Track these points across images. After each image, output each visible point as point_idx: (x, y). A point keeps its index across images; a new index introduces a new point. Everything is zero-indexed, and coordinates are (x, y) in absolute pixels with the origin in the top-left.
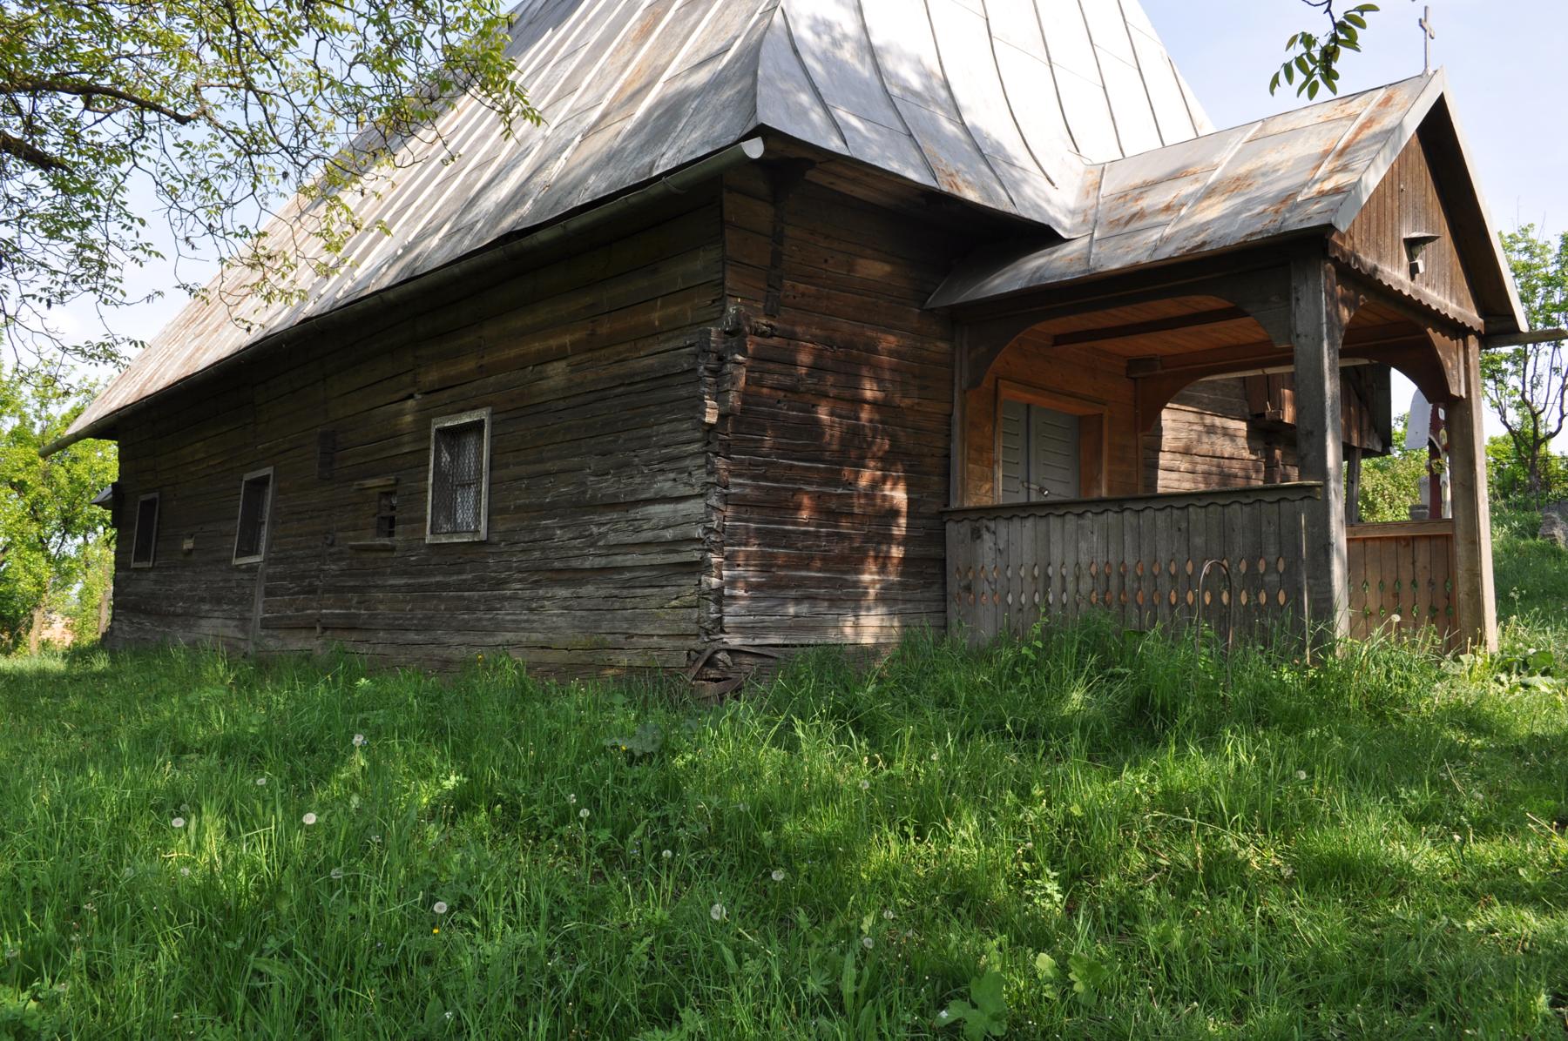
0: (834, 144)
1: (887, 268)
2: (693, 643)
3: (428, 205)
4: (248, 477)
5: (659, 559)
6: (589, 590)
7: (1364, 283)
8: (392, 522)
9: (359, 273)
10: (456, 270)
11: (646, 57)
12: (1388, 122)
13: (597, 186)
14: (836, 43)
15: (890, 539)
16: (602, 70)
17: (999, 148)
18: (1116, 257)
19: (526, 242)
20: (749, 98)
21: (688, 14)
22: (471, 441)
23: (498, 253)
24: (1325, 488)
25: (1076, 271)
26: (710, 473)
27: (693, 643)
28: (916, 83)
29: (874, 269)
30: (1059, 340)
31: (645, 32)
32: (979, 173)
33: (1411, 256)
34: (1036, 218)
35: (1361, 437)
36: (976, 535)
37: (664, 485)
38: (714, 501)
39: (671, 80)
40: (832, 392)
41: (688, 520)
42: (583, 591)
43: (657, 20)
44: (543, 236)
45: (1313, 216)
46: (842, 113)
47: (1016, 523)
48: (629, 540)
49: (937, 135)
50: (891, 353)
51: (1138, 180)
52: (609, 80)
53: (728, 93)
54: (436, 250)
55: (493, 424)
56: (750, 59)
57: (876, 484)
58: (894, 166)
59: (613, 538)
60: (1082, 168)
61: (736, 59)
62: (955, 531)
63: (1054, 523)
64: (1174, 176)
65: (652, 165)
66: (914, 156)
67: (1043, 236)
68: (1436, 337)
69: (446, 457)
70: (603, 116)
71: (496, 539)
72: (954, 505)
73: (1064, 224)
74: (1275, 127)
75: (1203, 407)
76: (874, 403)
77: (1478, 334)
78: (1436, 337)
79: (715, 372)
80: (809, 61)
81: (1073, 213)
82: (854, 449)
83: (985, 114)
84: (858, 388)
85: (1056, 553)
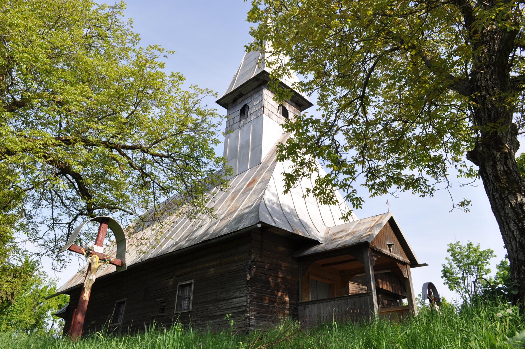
0: (273, 224)
1: (284, 249)
2: (243, 329)
3: (180, 233)
4: (117, 302)
5: (235, 311)
6: (218, 320)
7: (380, 253)
8: (163, 309)
9: (163, 248)
10: (192, 248)
11: (234, 205)
12: (380, 222)
13: (226, 231)
14: (273, 204)
15: (285, 309)
16: (223, 206)
17: (306, 224)
18: (330, 247)
19: (209, 242)
20: (258, 216)
21: (242, 196)
22: (188, 288)
23: (203, 244)
24: (372, 293)
25: (323, 250)
26: (248, 291)
27: (243, 329)
28: (288, 211)
29: (281, 249)
30: (323, 266)
31: (233, 199)
32: (303, 230)
33: (390, 248)
34: (314, 238)
35: (402, 293)
36: (305, 308)
37: (237, 294)
38: (248, 297)
39: (240, 210)
40: (272, 274)
41: (243, 301)
42: (217, 321)
43: (235, 196)
44: (213, 241)
45: (364, 240)
46: (274, 218)
47: (313, 305)
48: (227, 307)
49: (294, 222)
50: (285, 267)
51: (336, 232)
52: (225, 209)
53: (253, 215)
54: (184, 244)
55: (195, 283)
56: (257, 208)
57: (282, 295)
58: (285, 229)
59: (224, 307)
60: (325, 228)
61: (254, 207)
62: (300, 308)
63: (321, 304)
64: (343, 231)
65: (238, 228)
66: (289, 226)
67: (316, 243)
68: (399, 265)
69: (180, 292)
70: (225, 217)
71: (194, 310)
72: (300, 302)
73: (321, 240)
74: (362, 221)
75: (359, 283)
76: (281, 277)
77: (409, 264)
78: (399, 265)
79: (249, 269)
80: (268, 208)
81: (323, 238)
82: (277, 288)
83: (304, 217)
84: (278, 274)
85: (322, 311)
